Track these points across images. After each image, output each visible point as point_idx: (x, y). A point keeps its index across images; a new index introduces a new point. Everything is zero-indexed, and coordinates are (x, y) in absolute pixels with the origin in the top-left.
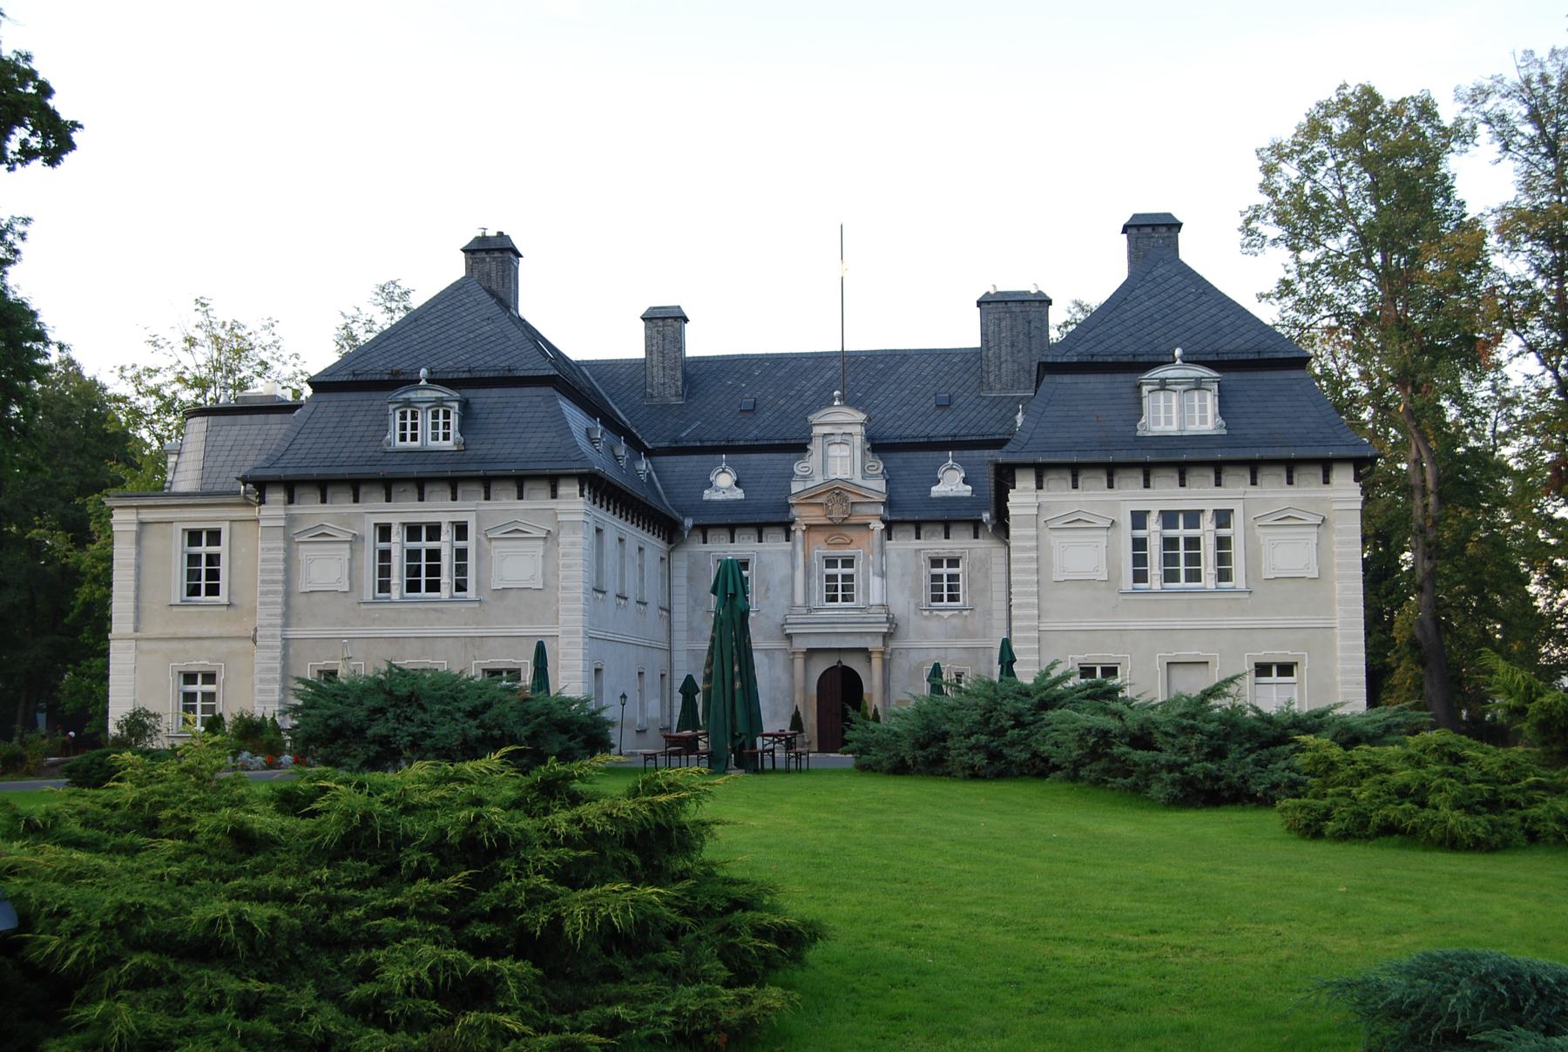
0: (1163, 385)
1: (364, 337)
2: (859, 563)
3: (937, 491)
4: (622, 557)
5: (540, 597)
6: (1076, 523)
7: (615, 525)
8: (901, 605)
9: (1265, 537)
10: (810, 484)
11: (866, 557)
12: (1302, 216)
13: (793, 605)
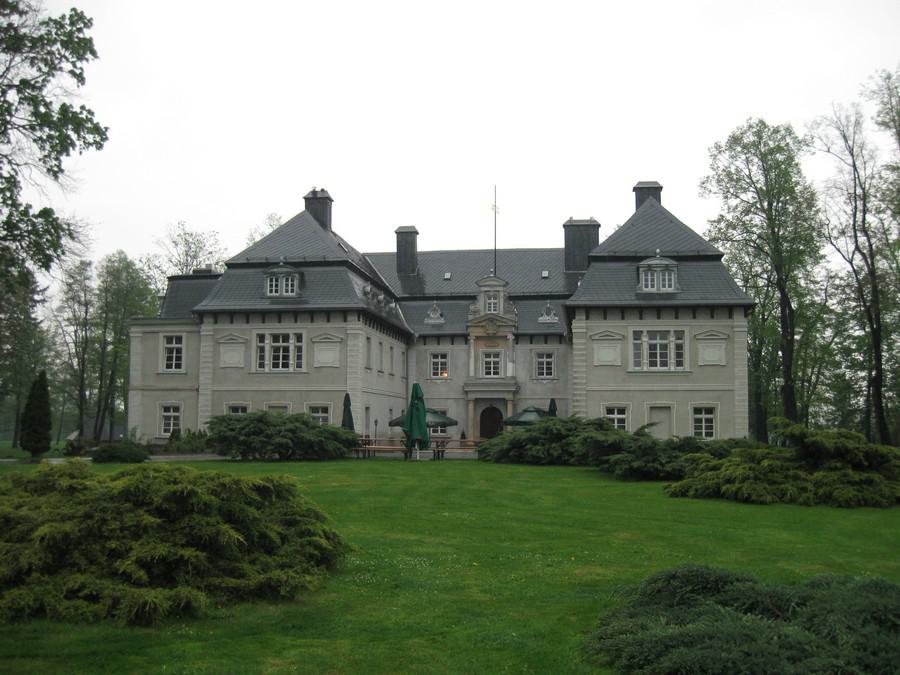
1: (258, 238)
2: (502, 356)
4: (381, 351)
5: (339, 372)
7: (377, 336)
8: (522, 377)
9: (700, 345)
11: (505, 353)
12: (732, 182)
13: (468, 376)
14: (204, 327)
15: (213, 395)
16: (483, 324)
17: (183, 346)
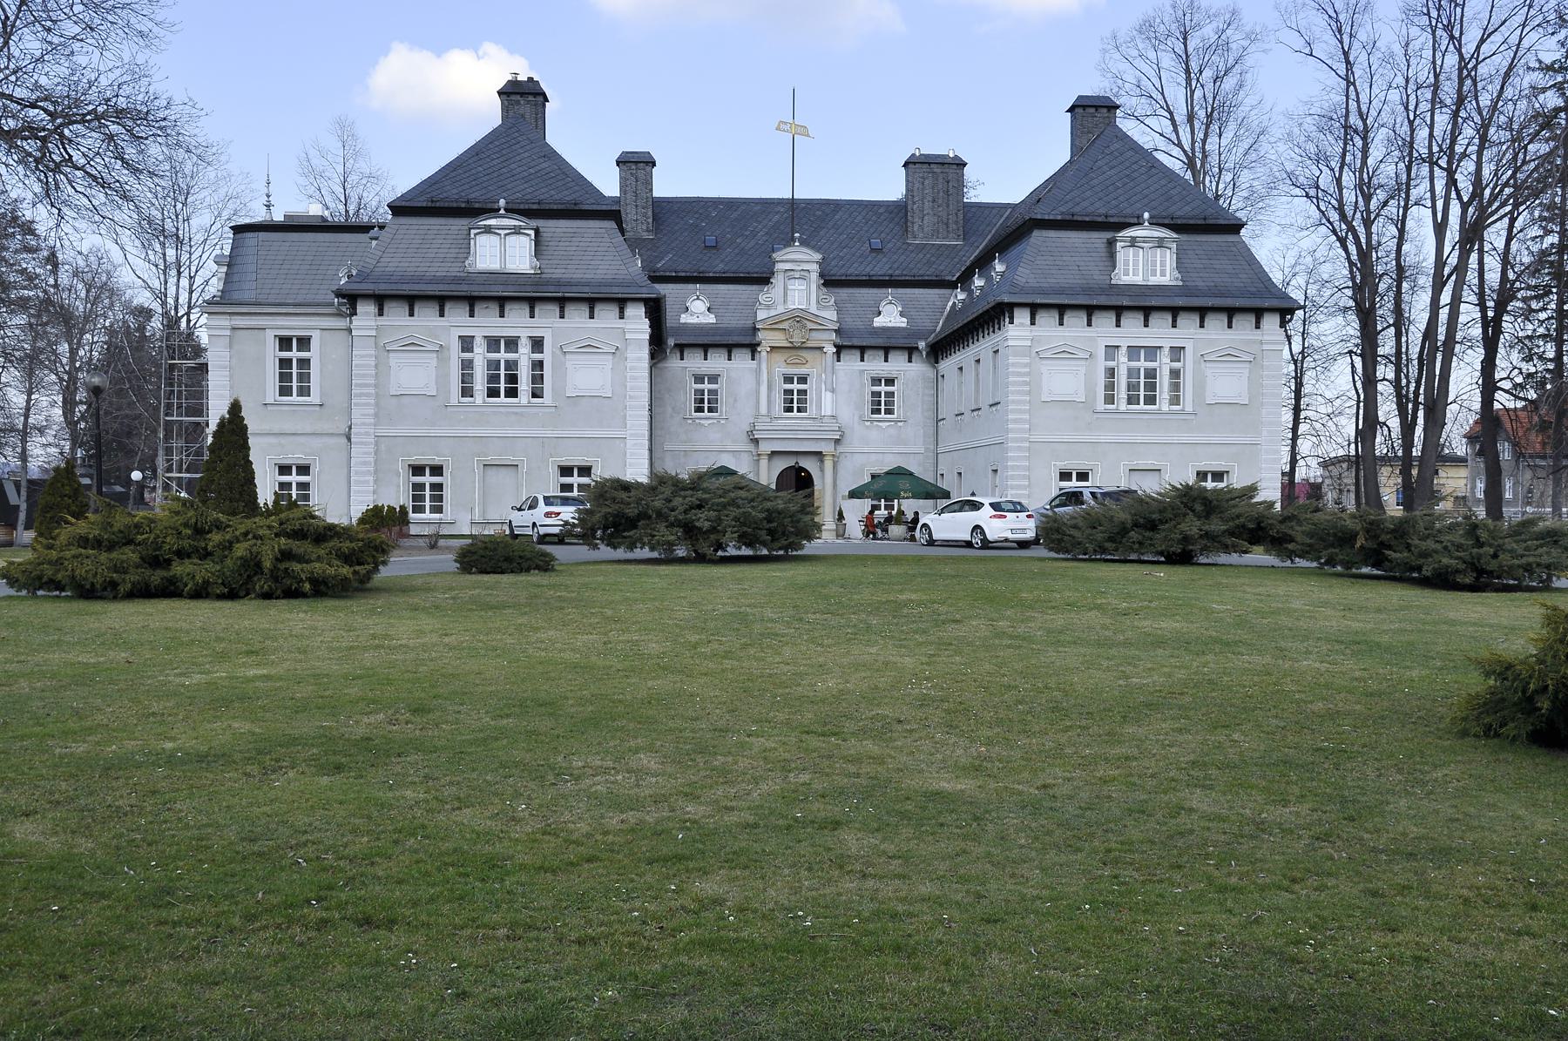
0: (1133, 242)
3: (879, 322)
8: (848, 416)
9: (1209, 370)
10: (773, 313)
14: (356, 321)
15: (377, 444)
16: (785, 325)
17: (313, 354)
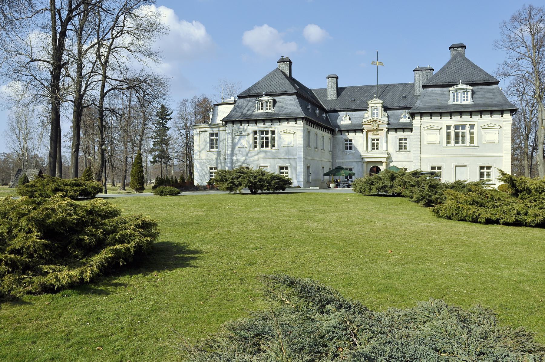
6: (431, 128)
